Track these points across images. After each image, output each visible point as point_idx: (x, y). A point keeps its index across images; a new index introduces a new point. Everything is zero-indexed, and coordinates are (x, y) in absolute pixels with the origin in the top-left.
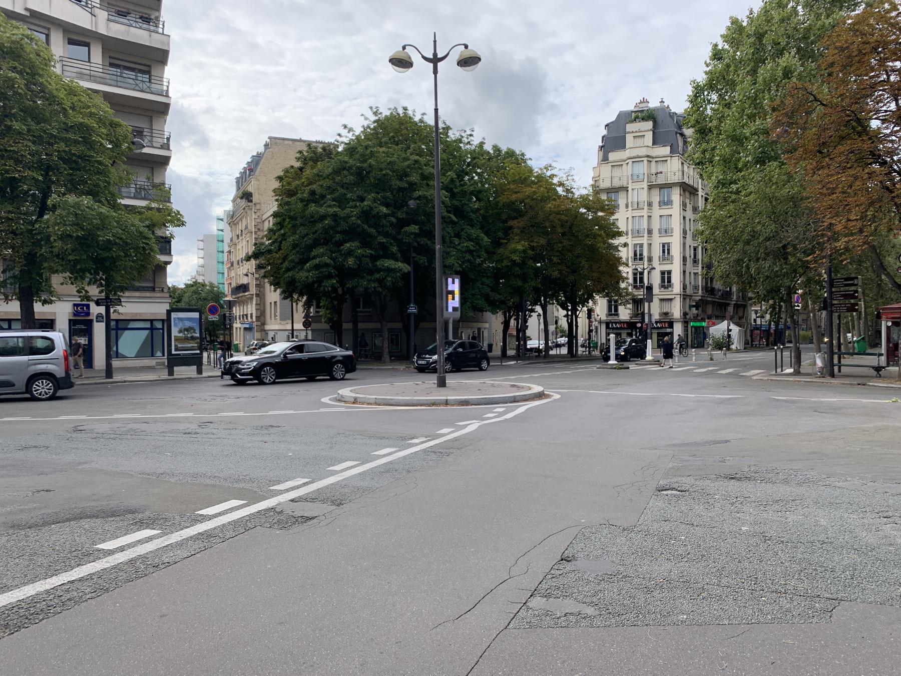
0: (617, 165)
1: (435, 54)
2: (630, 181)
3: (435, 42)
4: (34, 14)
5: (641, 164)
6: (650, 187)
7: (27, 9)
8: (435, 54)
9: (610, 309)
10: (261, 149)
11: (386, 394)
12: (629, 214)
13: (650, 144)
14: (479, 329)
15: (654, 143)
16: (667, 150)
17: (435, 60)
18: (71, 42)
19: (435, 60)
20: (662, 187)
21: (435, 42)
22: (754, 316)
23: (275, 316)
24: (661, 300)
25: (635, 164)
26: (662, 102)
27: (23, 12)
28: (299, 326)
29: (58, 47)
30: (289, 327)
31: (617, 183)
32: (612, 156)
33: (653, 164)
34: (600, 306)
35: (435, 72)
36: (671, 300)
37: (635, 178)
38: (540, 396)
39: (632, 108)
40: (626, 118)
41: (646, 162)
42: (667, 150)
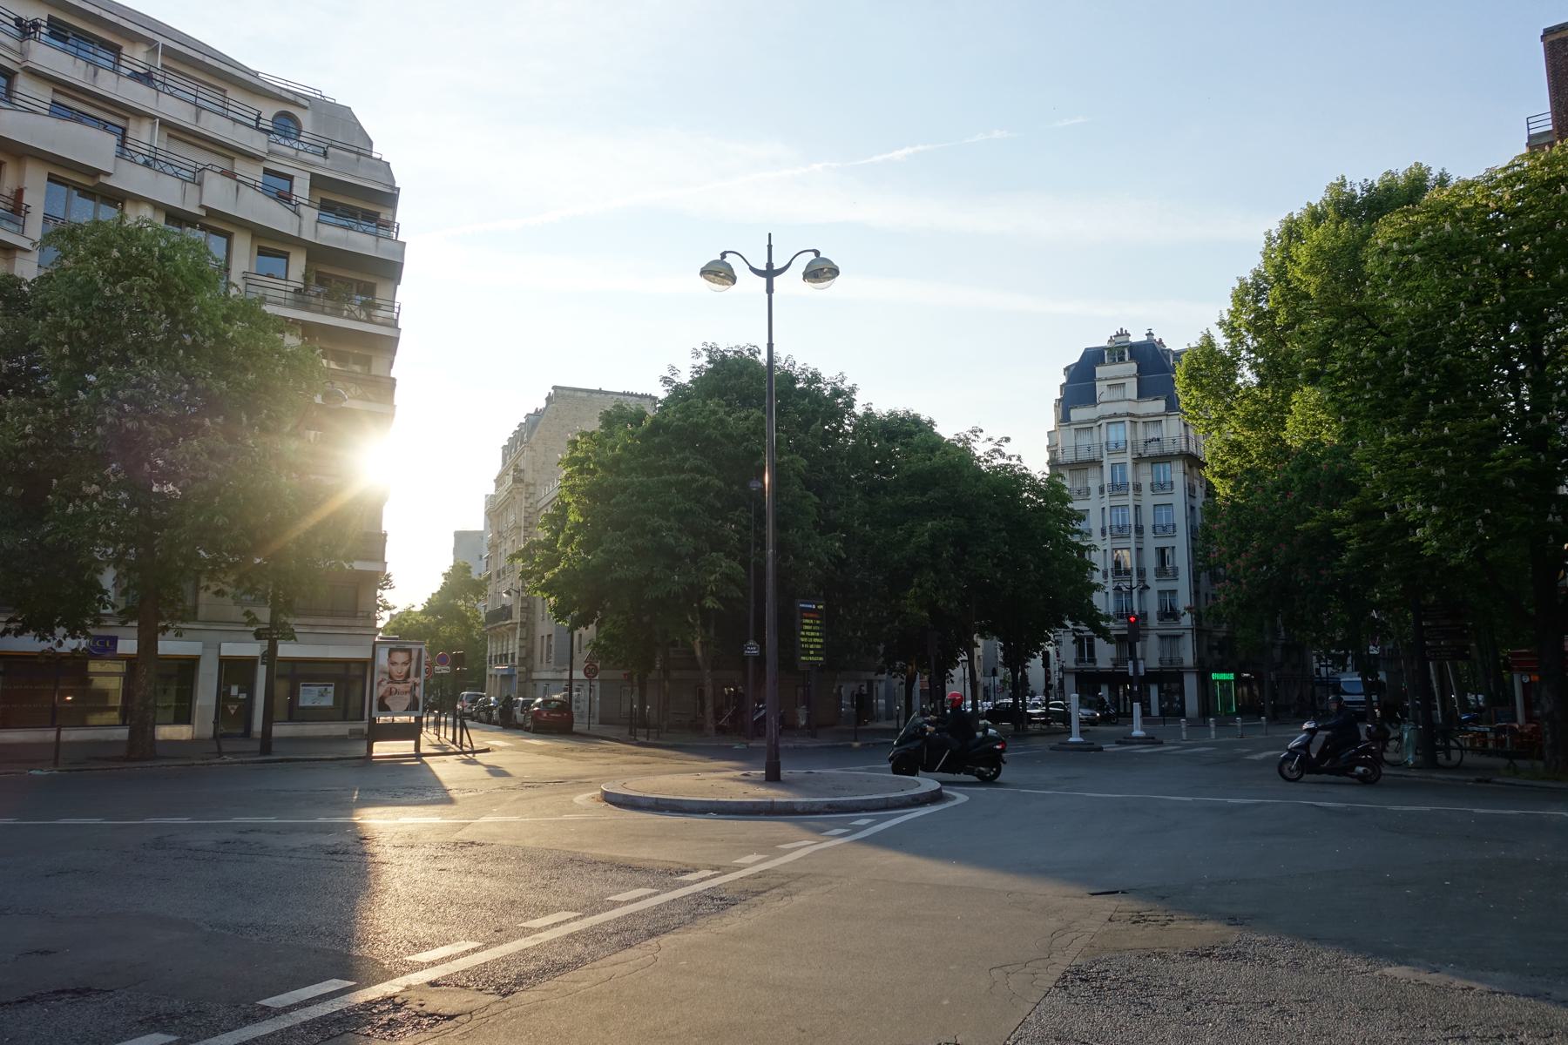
0: (1086, 427)
1: (770, 265)
2: (1105, 453)
3: (770, 247)
4: (212, 213)
5: (1121, 426)
6: (1139, 460)
7: (202, 207)
8: (770, 265)
9: (1080, 651)
10: (542, 404)
11: (882, 791)
12: (1107, 502)
13: (1135, 396)
14: (870, 683)
15: (1139, 396)
16: (1160, 406)
17: (770, 273)
18: (262, 252)
19: (770, 273)
20: (1157, 460)
21: (770, 247)
22: (1316, 666)
23: (548, 657)
24: (1162, 637)
25: (1112, 427)
26: (1150, 334)
27: (197, 211)
28: (579, 674)
29: (243, 257)
30: (566, 675)
31: (1084, 455)
32: (1077, 414)
33: (1140, 427)
34: (1061, 648)
35: (770, 290)
36: (1177, 637)
37: (1112, 447)
38: (935, 797)
39: (1105, 343)
40: (1093, 358)
41: (1128, 424)
42: (1160, 406)
